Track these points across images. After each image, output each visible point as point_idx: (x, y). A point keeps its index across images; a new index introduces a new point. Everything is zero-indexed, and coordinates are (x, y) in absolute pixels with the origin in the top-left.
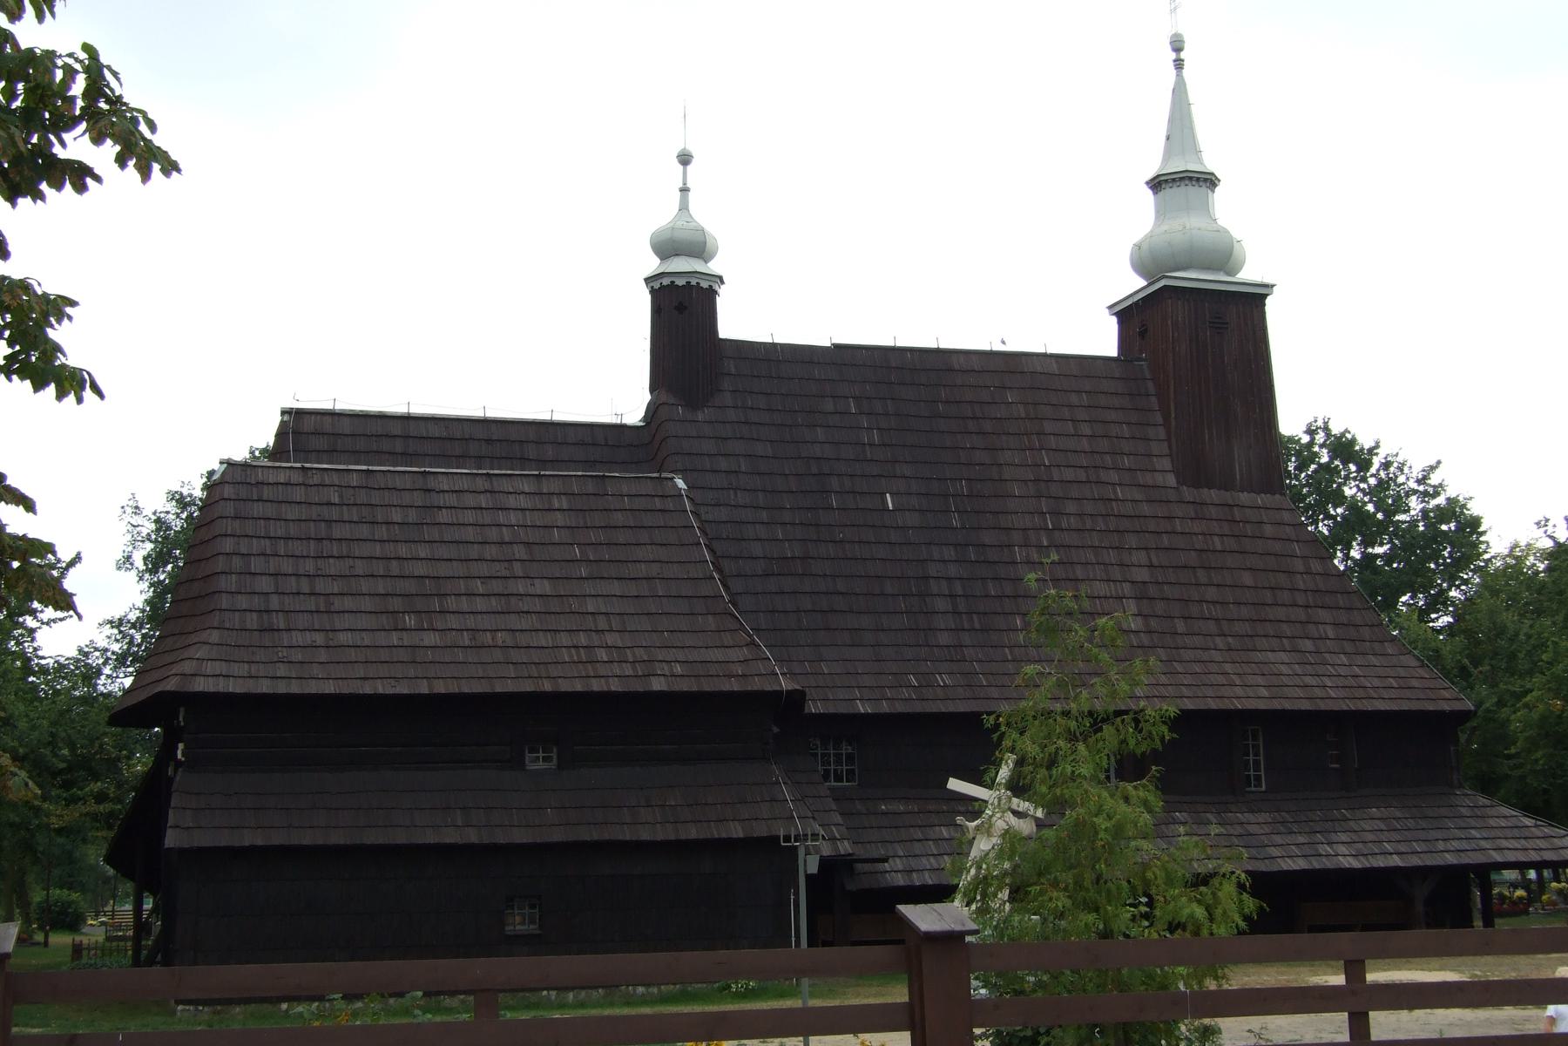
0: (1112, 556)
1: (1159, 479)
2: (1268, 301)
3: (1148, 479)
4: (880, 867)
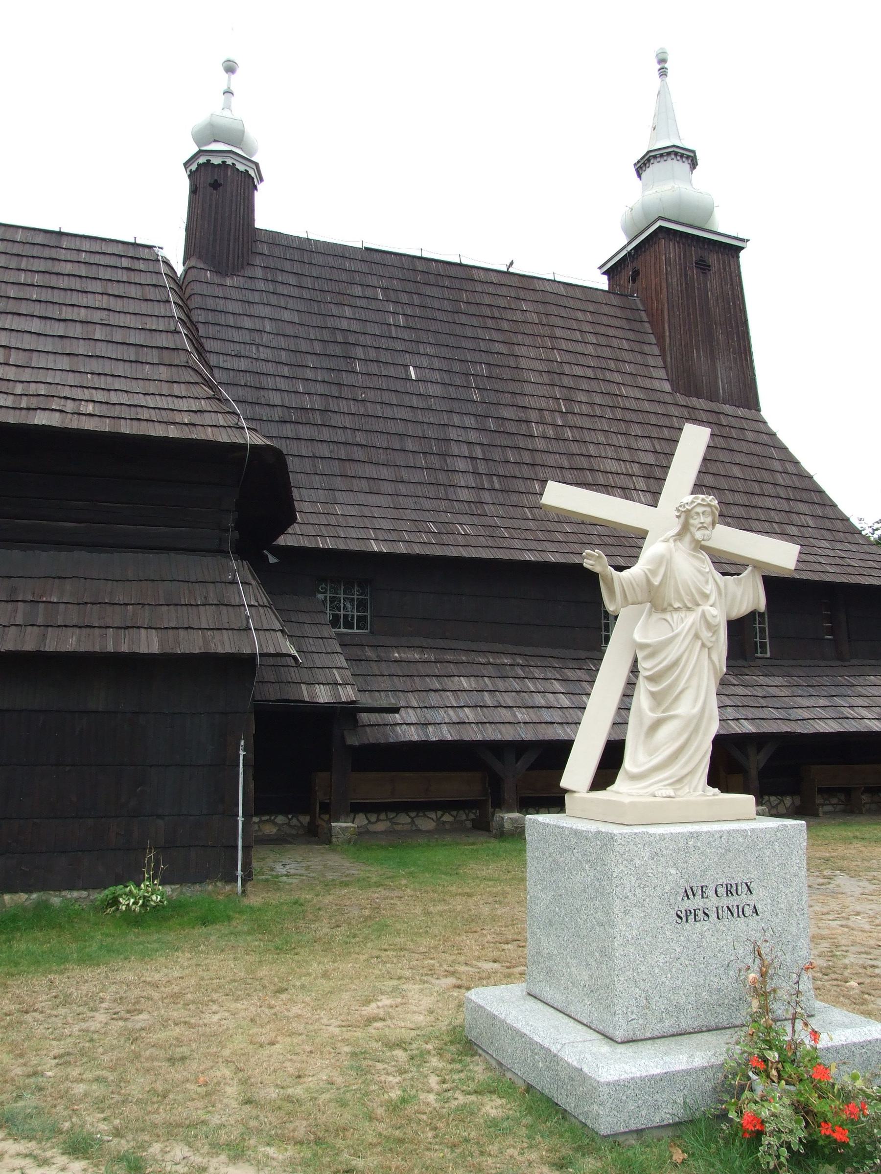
0: (621, 441)
1: (657, 385)
2: (742, 254)
3: (647, 383)
4: (390, 718)
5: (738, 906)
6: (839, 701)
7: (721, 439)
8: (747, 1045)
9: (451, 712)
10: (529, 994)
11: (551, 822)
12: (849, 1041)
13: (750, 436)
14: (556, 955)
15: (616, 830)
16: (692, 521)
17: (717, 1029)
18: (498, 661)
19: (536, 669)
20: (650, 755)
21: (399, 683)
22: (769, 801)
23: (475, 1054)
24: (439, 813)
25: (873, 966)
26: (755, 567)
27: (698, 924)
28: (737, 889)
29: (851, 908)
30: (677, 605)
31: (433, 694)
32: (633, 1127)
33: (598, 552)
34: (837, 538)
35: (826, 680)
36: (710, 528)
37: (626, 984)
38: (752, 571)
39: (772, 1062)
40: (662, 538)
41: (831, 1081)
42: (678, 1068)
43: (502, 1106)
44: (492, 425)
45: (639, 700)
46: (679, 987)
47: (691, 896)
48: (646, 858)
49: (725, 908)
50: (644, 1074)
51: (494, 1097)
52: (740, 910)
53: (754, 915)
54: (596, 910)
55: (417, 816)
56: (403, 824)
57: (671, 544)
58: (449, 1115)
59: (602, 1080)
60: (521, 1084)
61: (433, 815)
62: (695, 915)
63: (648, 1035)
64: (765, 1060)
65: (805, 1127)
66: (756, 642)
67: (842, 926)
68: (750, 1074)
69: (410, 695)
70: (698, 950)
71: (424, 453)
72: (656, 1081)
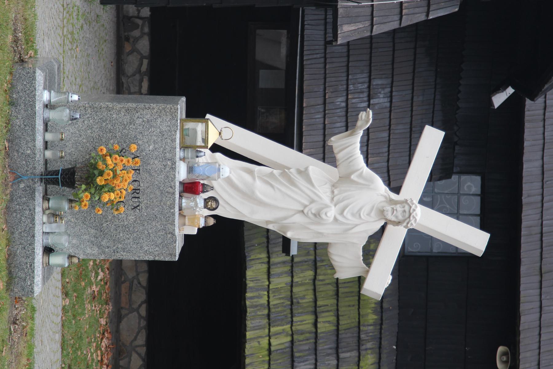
24: (143, 351)
28: (135, 197)
30: (336, 192)
50: (37, 97)
55: (140, 316)
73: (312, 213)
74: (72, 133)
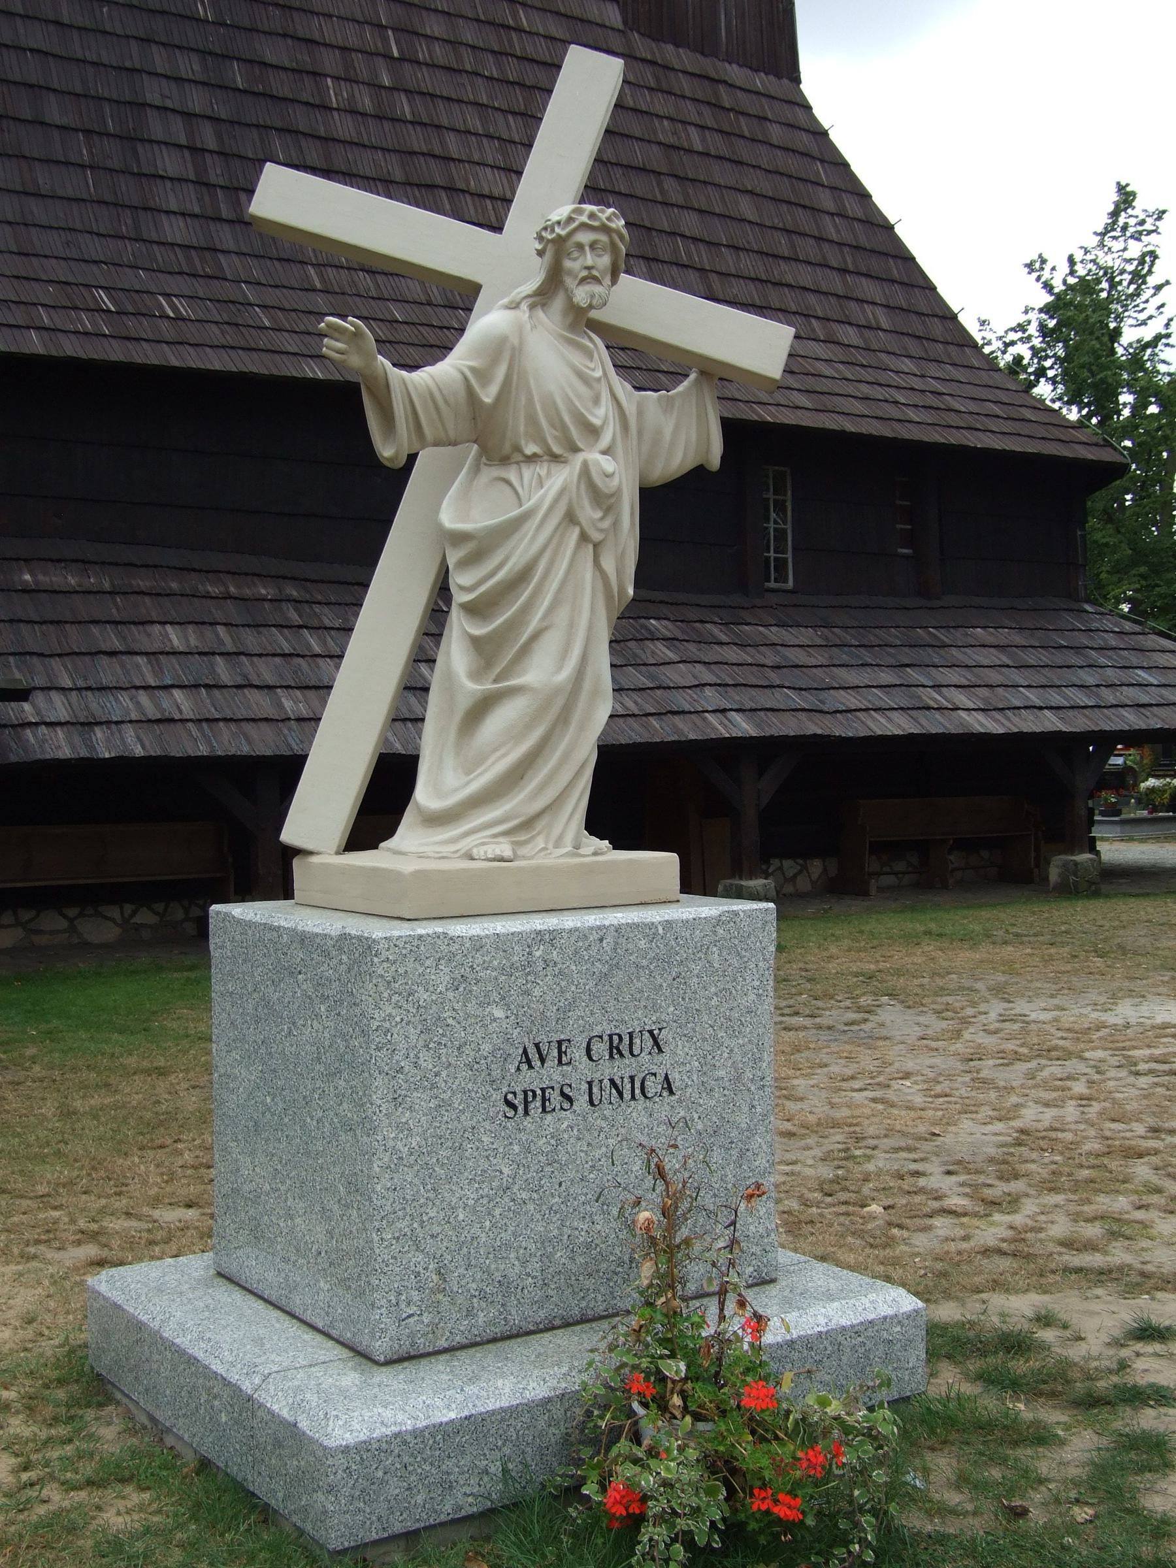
5: (632, 1078)
6: (914, 675)
7: (718, 137)
8: (629, 1351)
9: (143, 698)
10: (220, 1274)
11: (258, 919)
12: (832, 1325)
13: (776, 133)
14: (268, 1194)
15: (377, 930)
16: (568, 264)
17: (584, 1320)
18: (247, 592)
19: (326, 610)
20: (468, 772)
21: (32, 638)
22: (780, 868)
23: (109, 1400)
24: (128, 908)
25: (917, 1174)
26: (702, 373)
27: (549, 1117)
29: (897, 1065)
31: (104, 660)
32: (398, 1528)
33: (350, 324)
34: (932, 355)
35: (894, 636)
36: (607, 281)
37: (396, 1247)
38: (697, 380)
39: (674, 1382)
40: (505, 301)
41: (785, 1406)
42: (492, 1405)
43: (141, 1508)
44: (238, 76)
45: (448, 653)
46: (508, 1246)
47: (536, 1063)
48: (441, 988)
49: (606, 1082)
50: (420, 1424)
51: (129, 1489)
52: (637, 1085)
53: (665, 1094)
54: (341, 1097)
55: (81, 915)
56: (52, 933)
57: (523, 313)
58: (21, 1536)
59: (331, 1443)
60: (189, 1456)
61: (114, 912)
62: (544, 1100)
63: (443, 1343)
64: (662, 1379)
65: (727, 1499)
66: (768, 559)
67: (874, 1100)
68: (635, 1405)
69: (56, 663)
70: (548, 1169)
71: (88, 132)
72: (446, 1436)
73: (602, 519)
74: (468, 1267)
